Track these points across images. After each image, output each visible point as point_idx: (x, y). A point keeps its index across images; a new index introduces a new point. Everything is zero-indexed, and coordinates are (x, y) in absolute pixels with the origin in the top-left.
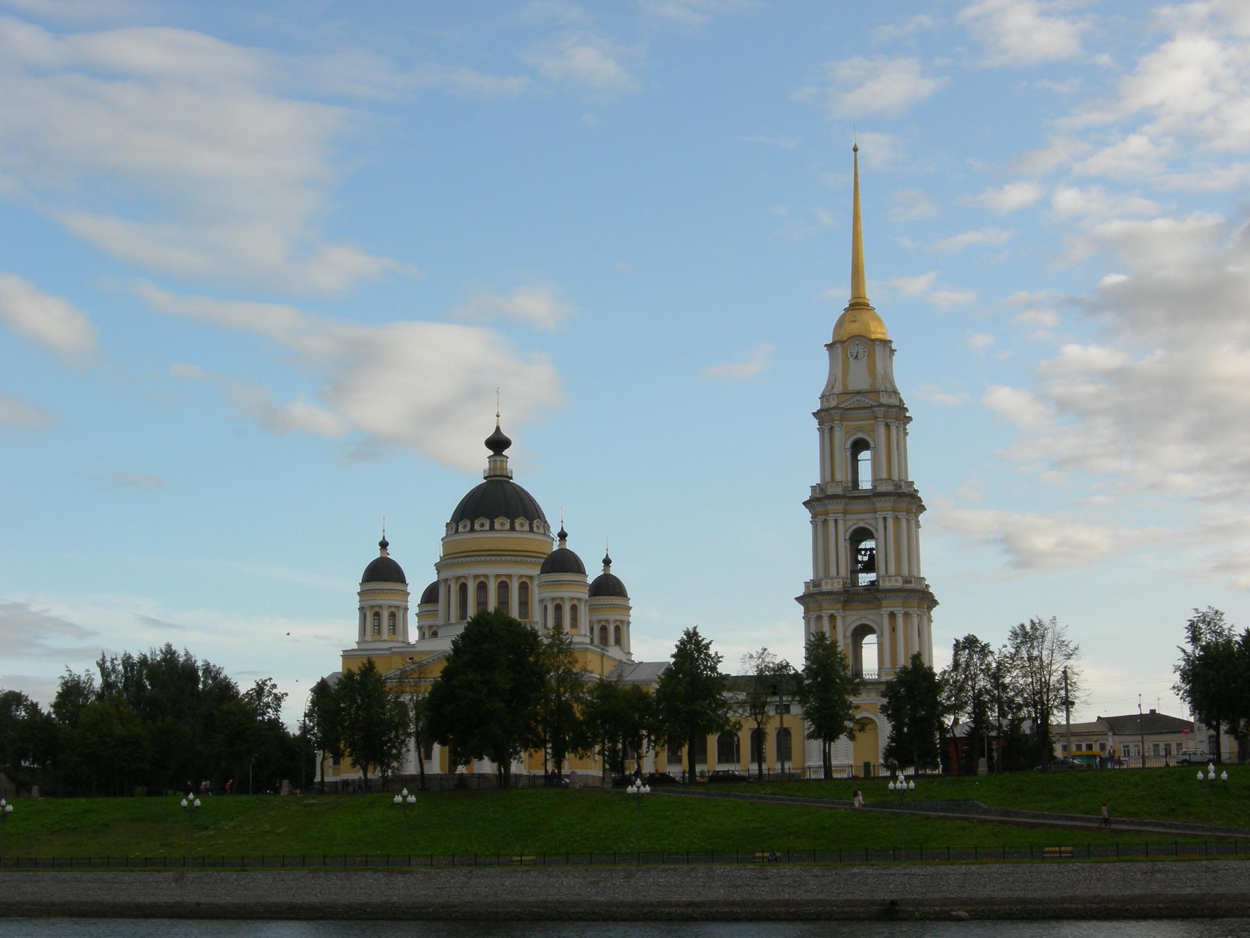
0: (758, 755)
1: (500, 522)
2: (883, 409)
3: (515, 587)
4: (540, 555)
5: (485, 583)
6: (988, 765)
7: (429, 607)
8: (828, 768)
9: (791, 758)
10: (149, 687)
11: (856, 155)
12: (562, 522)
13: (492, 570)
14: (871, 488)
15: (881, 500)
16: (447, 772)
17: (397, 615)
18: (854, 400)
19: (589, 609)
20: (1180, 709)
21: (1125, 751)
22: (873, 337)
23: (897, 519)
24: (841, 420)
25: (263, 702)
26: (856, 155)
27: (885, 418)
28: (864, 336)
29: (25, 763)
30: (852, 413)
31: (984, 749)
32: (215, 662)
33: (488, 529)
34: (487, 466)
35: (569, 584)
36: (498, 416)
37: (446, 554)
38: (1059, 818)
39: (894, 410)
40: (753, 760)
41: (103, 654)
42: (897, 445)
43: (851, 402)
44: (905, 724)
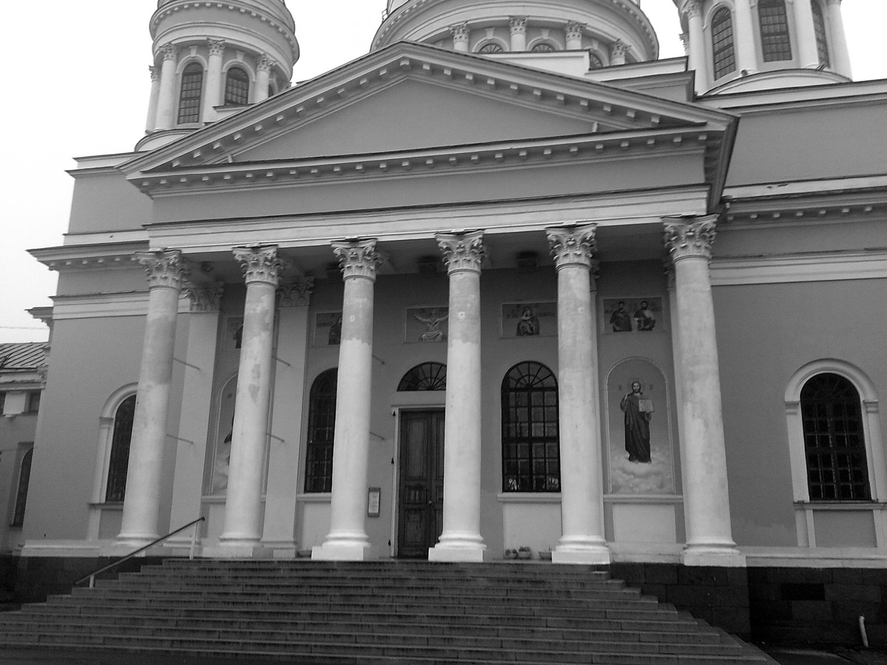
0: (190, 543)
3: (188, 546)
6: (814, 19)
7: (264, 500)
9: (51, 270)
10: (831, 446)
13: (203, 311)
14: (641, 410)
15: (127, 575)
16: (392, 551)
17: (252, 79)
19: (408, 313)
20: (724, 195)
22: (607, 548)
28: (237, 68)
32: (150, 77)
33: (370, 511)
37: (60, 294)
38: (429, 657)
40: (289, 37)
42: (853, 510)
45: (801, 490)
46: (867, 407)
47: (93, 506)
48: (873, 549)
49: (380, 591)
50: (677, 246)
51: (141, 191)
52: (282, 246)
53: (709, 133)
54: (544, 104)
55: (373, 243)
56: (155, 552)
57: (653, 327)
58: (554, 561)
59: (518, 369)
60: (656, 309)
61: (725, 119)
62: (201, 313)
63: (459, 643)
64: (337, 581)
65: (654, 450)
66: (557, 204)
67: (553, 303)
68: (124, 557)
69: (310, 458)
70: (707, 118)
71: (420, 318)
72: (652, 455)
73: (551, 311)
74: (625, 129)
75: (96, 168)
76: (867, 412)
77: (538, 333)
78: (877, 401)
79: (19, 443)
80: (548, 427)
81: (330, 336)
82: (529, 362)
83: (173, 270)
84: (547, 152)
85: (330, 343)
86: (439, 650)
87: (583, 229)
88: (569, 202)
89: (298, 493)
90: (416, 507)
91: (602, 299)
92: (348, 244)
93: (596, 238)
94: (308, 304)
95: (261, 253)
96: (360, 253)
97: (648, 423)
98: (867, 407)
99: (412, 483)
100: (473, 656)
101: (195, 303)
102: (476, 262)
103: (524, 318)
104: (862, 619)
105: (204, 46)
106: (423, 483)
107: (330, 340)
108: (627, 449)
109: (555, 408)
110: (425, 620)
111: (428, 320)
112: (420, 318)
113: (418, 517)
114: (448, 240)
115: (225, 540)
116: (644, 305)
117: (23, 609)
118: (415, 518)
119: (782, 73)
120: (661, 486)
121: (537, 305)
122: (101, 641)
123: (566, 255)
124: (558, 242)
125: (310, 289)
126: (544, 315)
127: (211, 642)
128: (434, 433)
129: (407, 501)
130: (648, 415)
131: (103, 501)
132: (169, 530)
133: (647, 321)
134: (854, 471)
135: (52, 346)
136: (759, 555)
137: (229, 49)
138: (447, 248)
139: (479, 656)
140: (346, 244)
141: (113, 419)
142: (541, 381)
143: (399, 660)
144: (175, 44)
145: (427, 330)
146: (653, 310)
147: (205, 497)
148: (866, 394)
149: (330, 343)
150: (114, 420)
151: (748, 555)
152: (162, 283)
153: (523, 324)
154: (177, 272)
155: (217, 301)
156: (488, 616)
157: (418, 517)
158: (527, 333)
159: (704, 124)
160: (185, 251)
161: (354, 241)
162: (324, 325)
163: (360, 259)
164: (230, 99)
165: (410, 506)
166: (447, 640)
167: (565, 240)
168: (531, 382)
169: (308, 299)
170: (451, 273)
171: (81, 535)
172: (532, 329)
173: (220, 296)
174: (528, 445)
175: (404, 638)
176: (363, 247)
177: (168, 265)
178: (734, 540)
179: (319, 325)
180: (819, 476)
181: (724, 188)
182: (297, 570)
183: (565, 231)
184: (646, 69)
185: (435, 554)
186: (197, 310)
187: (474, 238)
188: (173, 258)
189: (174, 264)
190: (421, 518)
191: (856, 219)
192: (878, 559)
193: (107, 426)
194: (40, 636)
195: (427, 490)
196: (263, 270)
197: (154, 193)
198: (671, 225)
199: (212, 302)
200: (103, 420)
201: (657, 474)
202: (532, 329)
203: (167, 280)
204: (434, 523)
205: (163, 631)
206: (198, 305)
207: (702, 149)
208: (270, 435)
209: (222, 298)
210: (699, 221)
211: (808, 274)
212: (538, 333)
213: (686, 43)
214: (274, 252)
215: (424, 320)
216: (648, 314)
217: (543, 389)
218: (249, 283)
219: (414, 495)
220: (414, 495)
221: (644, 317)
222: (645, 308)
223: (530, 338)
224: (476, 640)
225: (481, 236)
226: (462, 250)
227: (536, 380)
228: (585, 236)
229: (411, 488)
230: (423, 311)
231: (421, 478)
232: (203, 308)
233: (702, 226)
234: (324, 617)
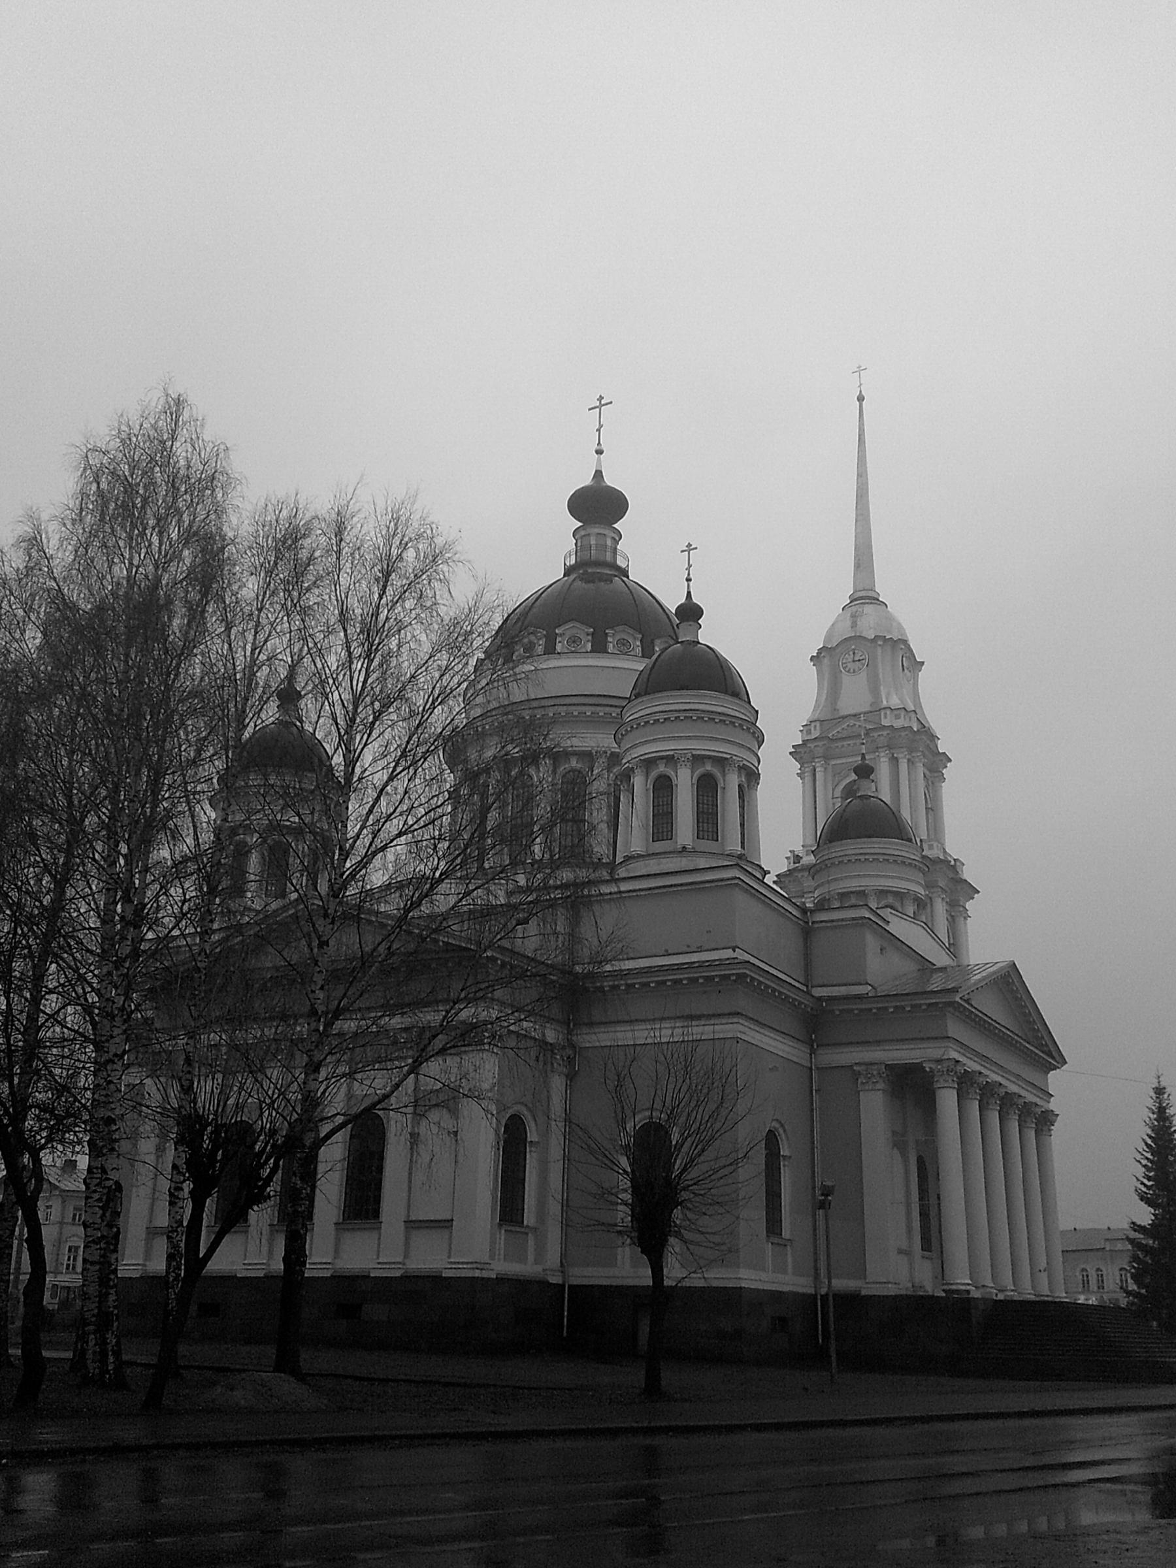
1: (568, 634)
2: (885, 733)
3: (684, 782)
4: (558, 701)
5: (669, 778)
8: (198, 845)
11: (861, 406)
12: (689, 580)
18: (844, 726)
21: (75, 1215)
23: (894, 761)
24: (827, 758)
25: (583, 984)
26: (861, 406)
27: (890, 747)
29: (252, 839)
30: (843, 746)
31: (564, 1298)
33: (589, 648)
34: (571, 543)
35: (419, 1228)
36: (599, 452)
39: (903, 734)
41: (1159, 1091)
43: (839, 729)
44: (97, 1015)
51: (936, 763)
105: (670, 760)
137: (698, 759)
180: (568, 1315)
208: (859, 371)
213: (1085, 1274)
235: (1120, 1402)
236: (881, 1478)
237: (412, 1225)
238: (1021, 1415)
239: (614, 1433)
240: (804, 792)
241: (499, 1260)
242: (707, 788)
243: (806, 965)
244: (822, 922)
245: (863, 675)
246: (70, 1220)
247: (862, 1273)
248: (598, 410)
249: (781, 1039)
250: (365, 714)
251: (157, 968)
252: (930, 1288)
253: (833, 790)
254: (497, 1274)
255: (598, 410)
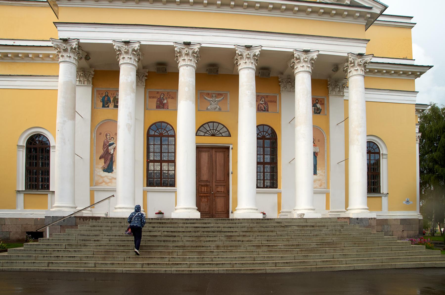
9: (113, 171)
45: (22, 186)
46: (383, 156)
47: (19, 192)
48: (380, 212)
49: (233, 242)
50: (180, 59)
52: (143, 43)
53: (371, 13)
54: (311, 15)
55: (198, 46)
56: (86, 214)
57: (321, 112)
58: (23, 194)
59: (263, 127)
60: (322, 104)
61: (381, 7)
62: (81, 86)
63: (312, 258)
64: (84, 237)
65: (319, 170)
66: (299, 39)
67: (276, 96)
68: (66, 217)
69: (276, 148)
70: (373, 5)
71: (207, 98)
72: (317, 172)
73: (174, 96)
74: (324, 2)
75: (401, 22)
76: (383, 158)
77: (268, 111)
78: (387, 153)
79: (100, 159)
80: (59, 229)
81: (157, 104)
82: (263, 125)
83: (74, 53)
84: (393, 72)
85: (157, 108)
86: (307, 262)
87: (134, 44)
88: (304, 38)
89: (144, 187)
90: (204, 195)
91: (95, 90)
92: (184, 46)
93: (260, 55)
94: (145, 85)
95: (130, 46)
96: (191, 52)
97: (317, 157)
98: (383, 156)
99: (202, 184)
100: (325, 263)
101: (78, 80)
102: (194, 61)
103: (261, 102)
104: (200, 60)
106: (208, 184)
107: (157, 106)
108: (196, 206)
109: (173, 154)
110: (283, 247)
111: (211, 99)
112: (207, 98)
113: (206, 200)
114: (241, 50)
115: (116, 208)
116: (317, 101)
117: (24, 246)
118: (204, 200)
119: (31, 50)
120: (321, 186)
121: (267, 96)
122: (93, 265)
123: (124, 58)
124: (119, 50)
125: (146, 76)
126: (271, 101)
127: (147, 257)
128: (214, 159)
129: (200, 192)
130: (317, 153)
131: (24, 189)
132: (187, 221)
133: (318, 109)
134: (35, 162)
135: (21, 224)
136: (23, 213)
138: (241, 54)
139: (328, 263)
140: (182, 46)
141: (25, 146)
142: (216, 130)
143: (291, 268)
144: (49, 237)
145: (211, 104)
146: (320, 104)
147: (91, 187)
148: (383, 151)
149: (157, 108)
150: (25, 146)
151: (97, 89)
152: (68, 59)
153: (261, 106)
154: (76, 54)
155: (144, 80)
156: (316, 243)
157: (206, 200)
158: (262, 110)
159: (371, 8)
160: (81, 41)
161: (127, 43)
162: (153, 97)
163: (130, 53)
164: (376, 155)
165: (202, 195)
166: (64, 235)
167: (123, 49)
168: (371, 150)
169: (144, 82)
170: (181, 66)
171: (14, 207)
172: (265, 108)
173: (93, 76)
174: (153, 138)
175: (282, 257)
176: (71, 45)
177: (72, 48)
178: (368, 206)
179: (150, 97)
181: (376, 20)
182: (187, 223)
183: (302, 53)
184: (395, 18)
185: (421, 218)
186: (79, 83)
187: (255, 51)
188: (74, 45)
189: (75, 49)
190: (208, 200)
191: (326, 17)
192: (383, 215)
193: (22, 150)
194: (49, 263)
195: (210, 187)
196: (131, 57)
197: (59, 3)
198: (239, 50)
199: (88, 80)
200: (19, 147)
201: (319, 180)
202: (265, 108)
203: (70, 58)
204: (214, 203)
205: (59, 245)
206: (80, 81)
207: (365, 22)
209: (93, 78)
210: (132, 44)
211: (375, 98)
212: (268, 111)
214: (139, 46)
215: (209, 99)
216: (318, 106)
217: (169, 136)
218: (122, 64)
219: (204, 189)
220: (204, 189)
221: (317, 107)
222: (317, 103)
223: (264, 112)
224: (320, 255)
225: (260, 50)
226: (249, 56)
227: (214, 131)
228: (255, 53)
229: (202, 186)
230: (208, 94)
231: (207, 181)
232: (83, 83)
233: (365, 60)
234: (225, 248)
235: (374, 93)
236: (86, 254)
237: (266, 269)
238: (126, 208)
239: (120, 208)
240: (323, 40)
241: (45, 171)
242: (376, 176)
243: (127, 208)
244: (120, 208)
245: (42, 140)
246: (152, 158)
247: (147, 217)
248: (220, 133)
249: (8, 77)
250: (316, 188)
251: (11, 226)
252: (273, 214)
253: (166, 109)
254: (294, 214)
255: (220, 133)
